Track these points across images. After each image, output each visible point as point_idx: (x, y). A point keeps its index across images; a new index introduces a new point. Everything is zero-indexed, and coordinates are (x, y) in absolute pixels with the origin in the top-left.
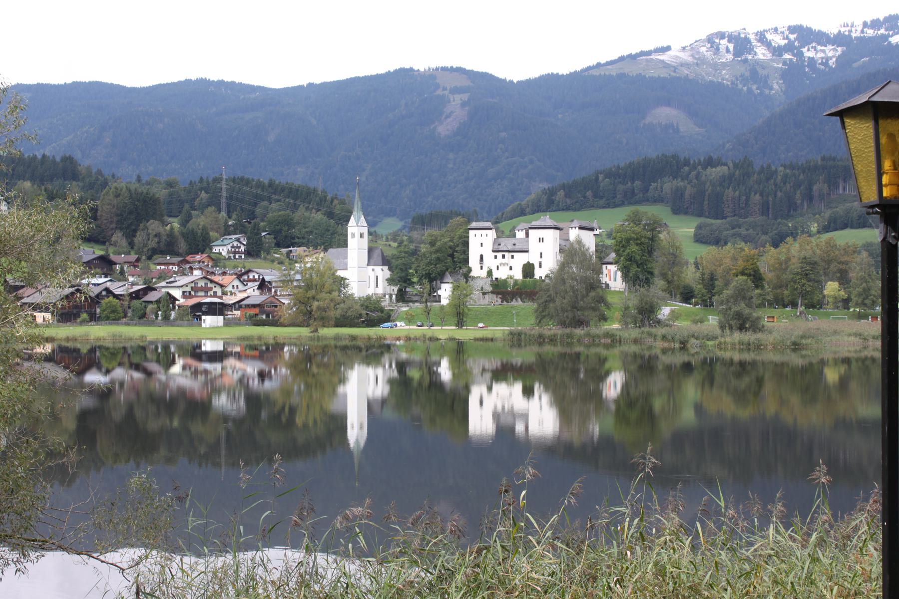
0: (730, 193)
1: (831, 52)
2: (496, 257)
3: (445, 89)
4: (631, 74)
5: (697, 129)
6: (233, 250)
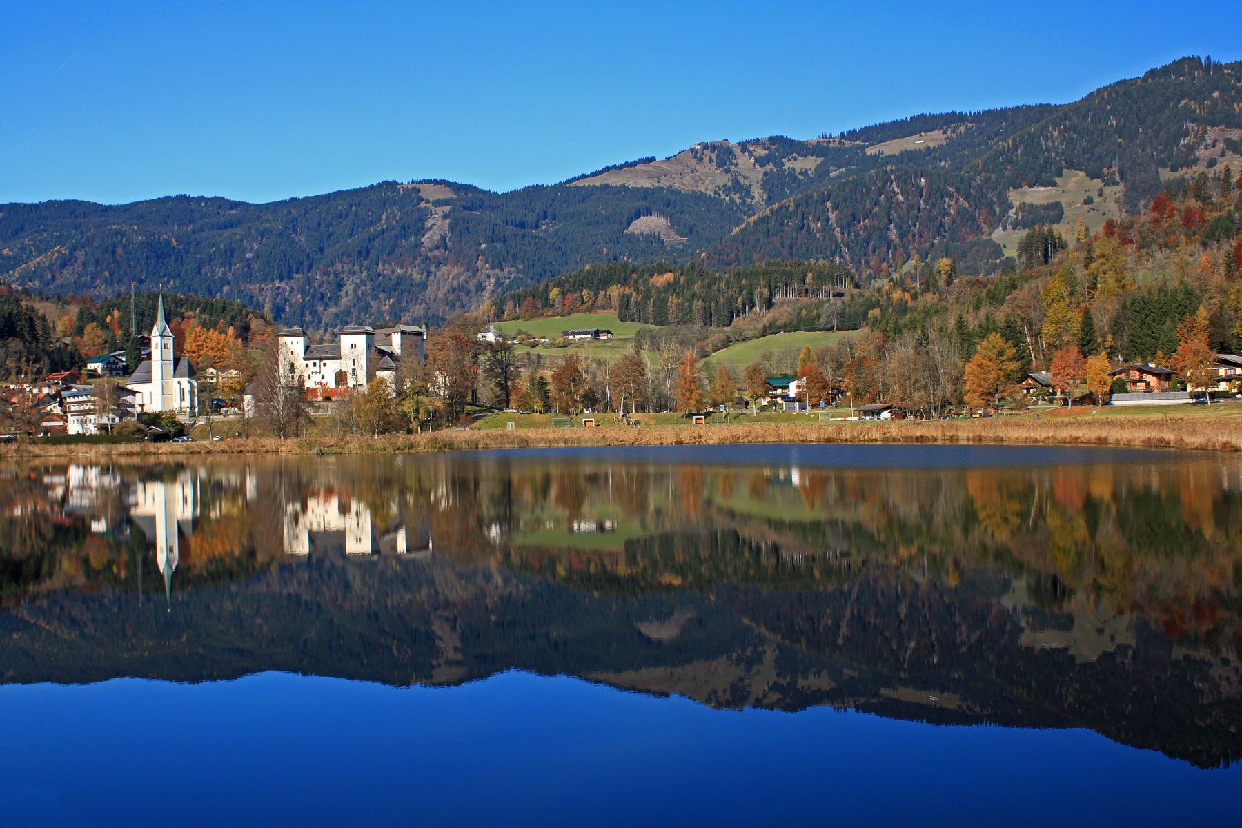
0: (673, 300)
1: (809, 163)
2: (307, 365)
3: (427, 202)
4: (614, 185)
5: (679, 238)
6: (109, 366)
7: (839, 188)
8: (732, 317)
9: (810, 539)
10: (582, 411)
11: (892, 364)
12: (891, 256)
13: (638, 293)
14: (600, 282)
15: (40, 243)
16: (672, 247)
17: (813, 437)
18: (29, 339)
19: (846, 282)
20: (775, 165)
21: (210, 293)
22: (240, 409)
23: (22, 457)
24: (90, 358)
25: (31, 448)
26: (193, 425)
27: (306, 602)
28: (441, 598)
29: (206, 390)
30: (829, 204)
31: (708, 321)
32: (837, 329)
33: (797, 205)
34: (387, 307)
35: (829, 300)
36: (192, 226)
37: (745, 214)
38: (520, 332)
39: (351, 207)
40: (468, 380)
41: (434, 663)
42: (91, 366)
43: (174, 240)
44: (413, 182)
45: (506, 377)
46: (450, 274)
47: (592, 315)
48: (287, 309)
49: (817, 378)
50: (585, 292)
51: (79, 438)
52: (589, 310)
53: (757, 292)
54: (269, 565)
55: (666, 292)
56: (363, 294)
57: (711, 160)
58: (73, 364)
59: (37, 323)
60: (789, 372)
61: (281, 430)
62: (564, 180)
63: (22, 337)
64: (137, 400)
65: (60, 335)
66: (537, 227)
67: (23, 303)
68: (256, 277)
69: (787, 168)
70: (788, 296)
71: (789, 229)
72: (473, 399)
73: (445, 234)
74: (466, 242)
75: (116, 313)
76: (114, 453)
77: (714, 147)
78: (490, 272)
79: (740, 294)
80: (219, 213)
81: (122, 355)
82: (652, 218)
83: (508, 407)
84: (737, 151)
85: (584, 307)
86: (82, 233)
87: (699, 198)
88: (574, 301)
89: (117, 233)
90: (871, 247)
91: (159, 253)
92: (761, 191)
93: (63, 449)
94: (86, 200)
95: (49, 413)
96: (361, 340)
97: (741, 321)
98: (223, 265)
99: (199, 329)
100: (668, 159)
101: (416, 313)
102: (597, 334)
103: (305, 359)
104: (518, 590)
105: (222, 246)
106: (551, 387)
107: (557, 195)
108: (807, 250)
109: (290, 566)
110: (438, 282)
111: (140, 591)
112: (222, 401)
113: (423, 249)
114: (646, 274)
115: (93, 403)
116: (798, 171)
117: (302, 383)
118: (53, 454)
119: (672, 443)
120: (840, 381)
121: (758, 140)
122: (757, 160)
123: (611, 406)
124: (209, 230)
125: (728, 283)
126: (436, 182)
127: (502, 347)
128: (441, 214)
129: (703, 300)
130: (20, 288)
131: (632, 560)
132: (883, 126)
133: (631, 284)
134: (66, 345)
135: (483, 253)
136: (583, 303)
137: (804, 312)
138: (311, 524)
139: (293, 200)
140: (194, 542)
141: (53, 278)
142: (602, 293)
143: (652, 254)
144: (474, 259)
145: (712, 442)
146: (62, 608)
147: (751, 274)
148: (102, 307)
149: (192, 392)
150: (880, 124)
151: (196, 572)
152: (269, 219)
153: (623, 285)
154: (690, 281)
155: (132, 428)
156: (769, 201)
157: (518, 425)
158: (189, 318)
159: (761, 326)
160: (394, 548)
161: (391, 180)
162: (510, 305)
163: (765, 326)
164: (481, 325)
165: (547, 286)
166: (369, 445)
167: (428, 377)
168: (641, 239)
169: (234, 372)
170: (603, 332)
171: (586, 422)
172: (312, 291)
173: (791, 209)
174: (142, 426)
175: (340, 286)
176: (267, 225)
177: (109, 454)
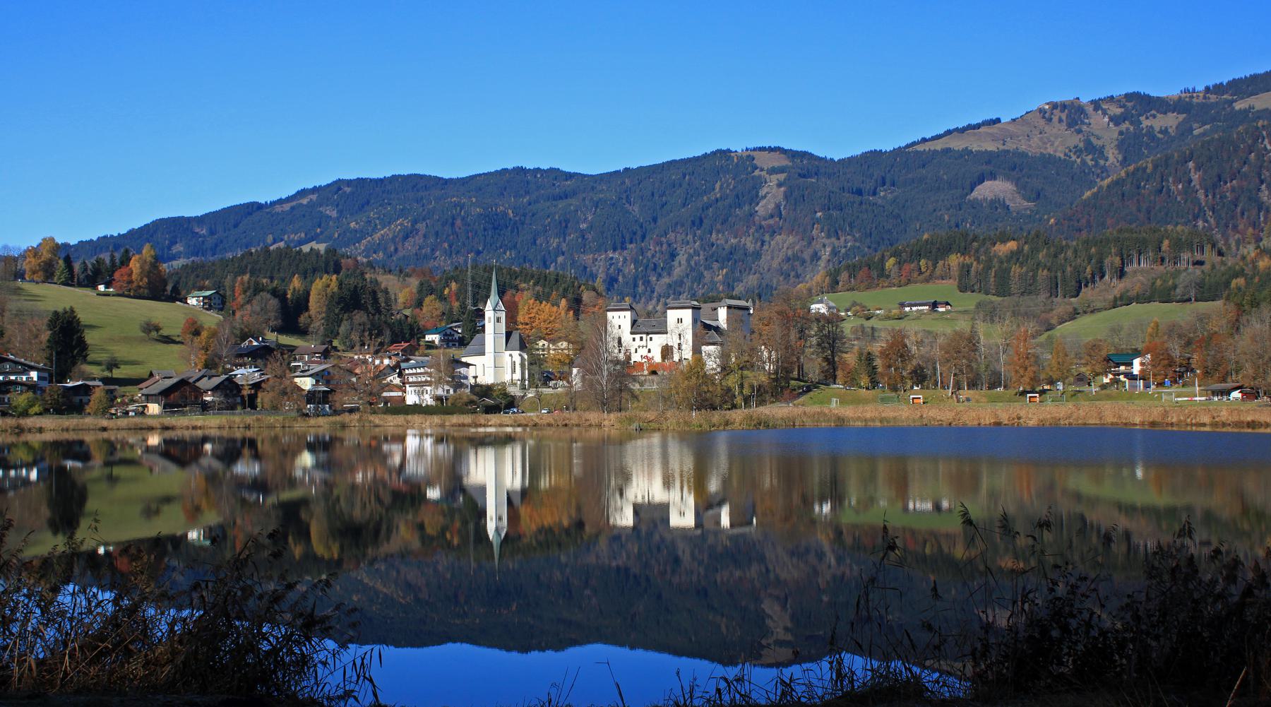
0: (1016, 270)
1: (1171, 121)
2: (634, 339)
3: (762, 170)
4: (956, 149)
6: (446, 338)
7: (1202, 146)
8: (1080, 287)
9: (1164, 527)
10: (912, 387)
11: (1244, 342)
12: (1262, 219)
13: (978, 263)
14: (940, 250)
15: (384, 216)
16: (1018, 214)
17: (1137, 420)
18: (373, 312)
19: (1207, 248)
20: (1132, 123)
21: (545, 263)
22: (568, 382)
23: (363, 426)
24: (427, 330)
25: (372, 418)
26: (523, 397)
27: (635, 576)
28: (772, 576)
29: (536, 364)
30: (1191, 164)
31: (1053, 291)
32: (1196, 300)
33: (1156, 167)
34: (721, 277)
35: (1187, 269)
36: (528, 198)
37: (1098, 176)
38: (854, 304)
39: (684, 176)
40: (793, 355)
41: (764, 642)
42: (429, 338)
43: (510, 212)
44: (747, 150)
45: (832, 352)
46: (784, 243)
47: (930, 286)
48: (620, 279)
49: (1163, 354)
50: (923, 262)
51: (417, 409)
52: (927, 281)
53: (1107, 261)
54: (597, 536)
55: (1008, 261)
56: (696, 264)
57: (1060, 121)
58: (412, 336)
59: (380, 295)
60: (1140, 346)
61: (605, 404)
62: (903, 145)
63: (366, 310)
64: (471, 372)
65: (400, 306)
66: (874, 194)
67: (367, 276)
68: (590, 247)
69: (1144, 126)
70: (1142, 265)
71: (1147, 192)
72: (799, 375)
73: (780, 202)
74: (801, 210)
75: (454, 285)
76: (447, 424)
77: (1064, 106)
78: (826, 241)
79: (1089, 263)
80: (554, 185)
81: (459, 327)
82: (997, 182)
83: (835, 384)
84: (1090, 109)
85: (920, 278)
86: (423, 206)
87: (1048, 160)
88: (911, 271)
89: (456, 205)
90: (1239, 209)
91: (495, 224)
92: (1116, 152)
93: (400, 419)
94: (427, 173)
95: (388, 385)
96: (687, 315)
97: (1090, 293)
98: (557, 236)
99: (531, 302)
100: (1014, 120)
101: (750, 283)
102: (934, 305)
103: (632, 333)
104: (851, 570)
105: (557, 217)
106: (878, 362)
107: (896, 160)
108: (1167, 214)
109: (618, 536)
110: (773, 251)
111: (472, 559)
112: (552, 373)
113: (757, 218)
114: (988, 244)
115: (430, 375)
116: (1157, 129)
117: (629, 358)
118: (391, 423)
119: (990, 424)
120: (1189, 359)
121: (1112, 97)
122: (1111, 119)
123: (942, 382)
124: (545, 201)
125: (1075, 251)
126: (771, 150)
127: (833, 320)
128: (776, 182)
129: (1049, 270)
130: (365, 260)
131: (970, 542)
132: (1254, 78)
133: (972, 253)
134: (407, 317)
135: (818, 221)
136: (921, 273)
137: (1159, 282)
138: (636, 497)
139: (626, 170)
140: (524, 511)
141: (396, 250)
142: (941, 263)
143: (997, 220)
144: (809, 227)
145: (1031, 423)
146: (398, 572)
147: (1101, 242)
148: (441, 279)
149: (522, 365)
150: (1251, 75)
151: (525, 541)
152: (603, 190)
153: (963, 254)
154: (1035, 250)
155: (465, 399)
156: (1124, 162)
157: (843, 402)
158: (523, 290)
159: (1111, 297)
160: (718, 522)
161: (724, 148)
162: (844, 276)
163: (1115, 297)
164: (810, 296)
165: (883, 256)
166: (686, 422)
167: (753, 350)
168: (984, 205)
169: (565, 344)
170: (941, 303)
171: (913, 398)
172: (645, 261)
173: (1148, 171)
174: (475, 398)
175: (673, 256)
176: (601, 196)
177: (442, 426)
